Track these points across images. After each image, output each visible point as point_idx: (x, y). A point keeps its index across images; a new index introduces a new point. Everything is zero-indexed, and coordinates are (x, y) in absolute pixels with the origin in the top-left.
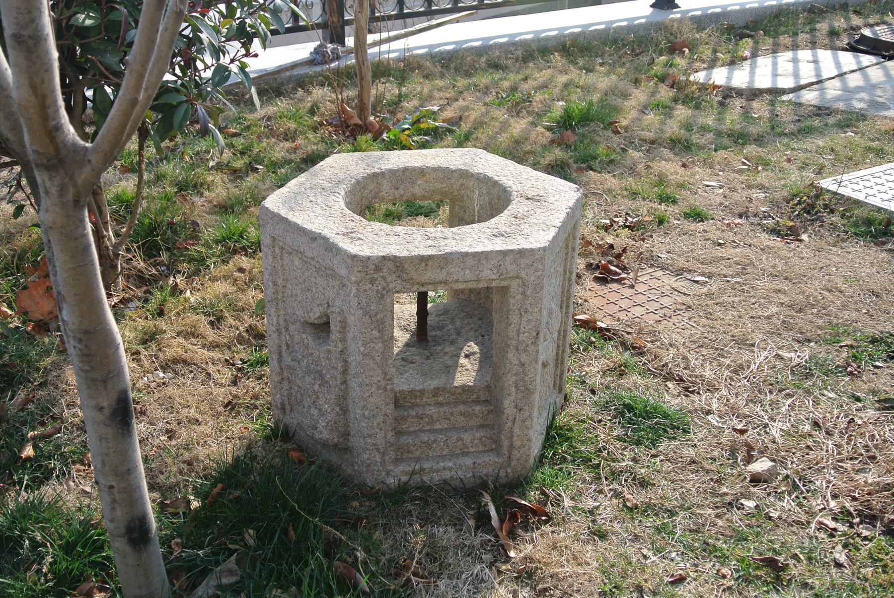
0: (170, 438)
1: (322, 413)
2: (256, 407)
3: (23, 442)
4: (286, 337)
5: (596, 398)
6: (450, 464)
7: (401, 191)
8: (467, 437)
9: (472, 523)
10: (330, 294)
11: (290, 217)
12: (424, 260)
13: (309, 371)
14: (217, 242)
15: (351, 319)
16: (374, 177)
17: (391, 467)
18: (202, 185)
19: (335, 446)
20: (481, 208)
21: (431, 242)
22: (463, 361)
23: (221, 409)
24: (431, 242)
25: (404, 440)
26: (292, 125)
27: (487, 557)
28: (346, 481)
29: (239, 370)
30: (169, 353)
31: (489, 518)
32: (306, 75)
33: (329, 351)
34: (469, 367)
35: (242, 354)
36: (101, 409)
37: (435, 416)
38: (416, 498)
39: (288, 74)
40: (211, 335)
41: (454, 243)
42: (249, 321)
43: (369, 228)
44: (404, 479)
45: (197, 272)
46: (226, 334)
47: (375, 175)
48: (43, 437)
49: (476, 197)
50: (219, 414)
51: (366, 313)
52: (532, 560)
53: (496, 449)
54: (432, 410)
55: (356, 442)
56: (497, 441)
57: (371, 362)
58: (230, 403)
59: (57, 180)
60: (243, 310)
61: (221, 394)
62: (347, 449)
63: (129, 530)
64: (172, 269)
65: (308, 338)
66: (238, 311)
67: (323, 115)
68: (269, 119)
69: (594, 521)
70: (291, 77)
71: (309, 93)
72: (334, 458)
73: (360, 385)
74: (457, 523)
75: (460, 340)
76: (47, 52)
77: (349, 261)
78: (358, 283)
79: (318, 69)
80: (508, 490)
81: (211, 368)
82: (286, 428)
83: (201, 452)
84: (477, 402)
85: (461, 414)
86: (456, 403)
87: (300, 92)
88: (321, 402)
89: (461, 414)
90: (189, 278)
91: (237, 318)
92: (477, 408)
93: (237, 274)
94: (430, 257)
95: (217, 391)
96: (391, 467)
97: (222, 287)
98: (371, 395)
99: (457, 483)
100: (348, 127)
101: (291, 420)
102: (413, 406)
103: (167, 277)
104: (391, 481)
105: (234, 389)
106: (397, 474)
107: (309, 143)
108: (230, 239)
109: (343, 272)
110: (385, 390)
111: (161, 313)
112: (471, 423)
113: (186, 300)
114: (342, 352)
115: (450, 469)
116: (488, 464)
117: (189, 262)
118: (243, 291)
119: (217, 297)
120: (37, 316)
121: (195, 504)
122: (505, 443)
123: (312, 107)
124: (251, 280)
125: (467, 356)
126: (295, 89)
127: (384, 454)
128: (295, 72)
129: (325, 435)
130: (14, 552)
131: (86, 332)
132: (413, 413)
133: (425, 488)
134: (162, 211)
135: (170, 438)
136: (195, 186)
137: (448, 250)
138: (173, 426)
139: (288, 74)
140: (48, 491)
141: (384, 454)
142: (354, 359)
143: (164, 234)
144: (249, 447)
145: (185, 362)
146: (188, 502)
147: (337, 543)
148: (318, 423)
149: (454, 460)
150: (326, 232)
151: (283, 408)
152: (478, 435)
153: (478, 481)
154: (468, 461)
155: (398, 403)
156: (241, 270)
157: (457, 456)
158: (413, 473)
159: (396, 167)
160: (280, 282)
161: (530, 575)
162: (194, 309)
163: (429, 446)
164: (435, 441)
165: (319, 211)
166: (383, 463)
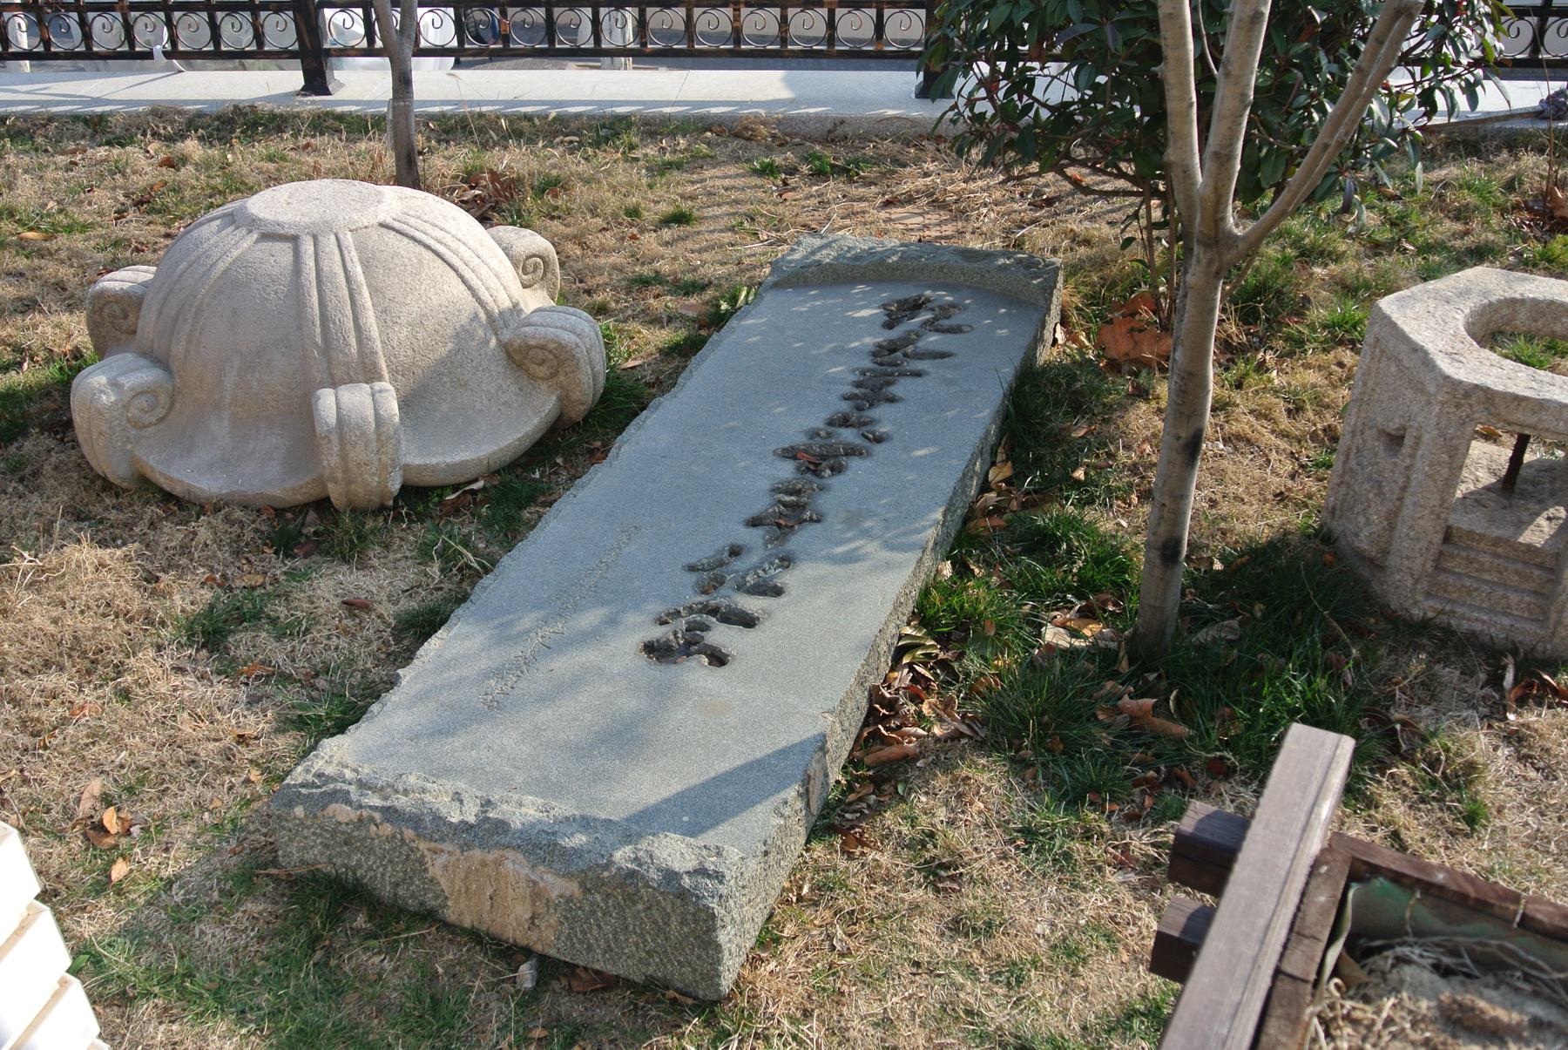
0: (1211, 507)
1: (1368, 523)
2: (1306, 506)
3: (1076, 466)
4: (1358, 441)
6: (1485, 618)
7: (1540, 324)
8: (1514, 598)
9: (1483, 676)
10: (1415, 408)
11: (1399, 323)
12: (1518, 400)
13: (1370, 479)
14: (1325, 327)
15: (1426, 437)
16: (1512, 302)
17: (1420, 598)
18: (1330, 253)
19: (1371, 560)
21: (1534, 384)
23: (1271, 497)
24: (1534, 384)
25: (1442, 577)
26: (1472, 199)
27: (1486, 710)
28: (1368, 597)
29: (1302, 466)
30: (1235, 427)
31: (1503, 678)
32: (1521, 132)
33: (1395, 464)
34: (1546, 529)
35: (1310, 452)
36: (1178, 438)
37: (1487, 565)
38: (1434, 636)
39: (1497, 125)
40: (1285, 423)
41: (1558, 391)
42: (1330, 420)
43: (1475, 354)
44: (1430, 614)
45: (1291, 354)
46: (1300, 426)
47: (1513, 301)
48: (1095, 467)
50: (1266, 501)
51: (1442, 435)
52: (1529, 728)
53: (1542, 622)
55: (1393, 561)
56: (1545, 613)
57: (1431, 484)
58: (1281, 493)
59: (1209, 255)
60: (1328, 407)
61: (1276, 483)
62: (1382, 568)
63: (1165, 546)
64: (1263, 342)
65: (1380, 447)
66: (1321, 405)
67: (1524, 193)
68: (1446, 186)
70: (1500, 130)
71: (1517, 159)
72: (1366, 574)
73: (1414, 504)
74: (1468, 672)
76: (1233, 167)
78: (1443, 404)
79: (1543, 125)
81: (1273, 456)
82: (1330, 531)
83: (1239, 527)
84: (1540, 566)
85: (1516, 572)
86: (1515, 561)
87: (1505, 155)
88: (1371, 511)
89: (1516, 572)
90: (1281, 358)
91: (1316, 413)
92: (1537, 572)
93: (1334, 367)
95: (1271, 478)
96: (1420, 598)
97: (1313, 377)
98: (1422, 518)
99: (1486, 639)
100: (1552, 218)
101: (1337, 526)
102: (1467, 548)
103: (1257, 350)
104: (1415, 611)
105: (1290, 483)
106: (1423, 608)
107: (1490, 229)
108: (1340, 327)
109: (1432, 389)
110: (1438, 516)
111: (1239, 386)
112: (1525, 586)
113: (1270, 380)
114: (1408, 468)
115: (1484, 622)
116: (1528, 632)
117: (1286, 340)
118: (1335, 387)
119: (1304, 386)
120: (1113, 354)
121: (1218, 566)
122: (1553, 616)
123: (1513, 179)
124: (1348, 378)
125: (1549, 519)
126: (1498, 150)
127: (1417, 581)
128: (1508, 125)
129: (1364, 544)
130: (1052, 549)
131: (1190, 374)
132: (1464, 554)
133: (1449, 632)
134: (1276, 274)
135: (1211, 507)
136: (1321, 254)
137: (1548, 396)
138: (1218, 497)
139: (1497, 125)
140: (1090, 514)
141: (1417, 581)
142: (1417, 477)
143: (1268, 302)
144: (1286, 533)
145: (1248, 441)
146: (1212, 563)
147: (1337, 639)
148: (1363, 532)
149: (1487, 613)
150: (1430, 347)
151: (1333, 512)
152: (1527, 599)
153: (1510, 646)
154: (1506, 622)
155: (1448, 537)
156: (1341, 365)
157: (1496, 613)
158: (1442, 612)
159: (1541, 297)
160: (1370, 383)
161: (1520, 740)
162: (1276, 392)
163: (1469, 593)
164: (1476, 590)
165: (1432, 324)
166: (1414, 590)
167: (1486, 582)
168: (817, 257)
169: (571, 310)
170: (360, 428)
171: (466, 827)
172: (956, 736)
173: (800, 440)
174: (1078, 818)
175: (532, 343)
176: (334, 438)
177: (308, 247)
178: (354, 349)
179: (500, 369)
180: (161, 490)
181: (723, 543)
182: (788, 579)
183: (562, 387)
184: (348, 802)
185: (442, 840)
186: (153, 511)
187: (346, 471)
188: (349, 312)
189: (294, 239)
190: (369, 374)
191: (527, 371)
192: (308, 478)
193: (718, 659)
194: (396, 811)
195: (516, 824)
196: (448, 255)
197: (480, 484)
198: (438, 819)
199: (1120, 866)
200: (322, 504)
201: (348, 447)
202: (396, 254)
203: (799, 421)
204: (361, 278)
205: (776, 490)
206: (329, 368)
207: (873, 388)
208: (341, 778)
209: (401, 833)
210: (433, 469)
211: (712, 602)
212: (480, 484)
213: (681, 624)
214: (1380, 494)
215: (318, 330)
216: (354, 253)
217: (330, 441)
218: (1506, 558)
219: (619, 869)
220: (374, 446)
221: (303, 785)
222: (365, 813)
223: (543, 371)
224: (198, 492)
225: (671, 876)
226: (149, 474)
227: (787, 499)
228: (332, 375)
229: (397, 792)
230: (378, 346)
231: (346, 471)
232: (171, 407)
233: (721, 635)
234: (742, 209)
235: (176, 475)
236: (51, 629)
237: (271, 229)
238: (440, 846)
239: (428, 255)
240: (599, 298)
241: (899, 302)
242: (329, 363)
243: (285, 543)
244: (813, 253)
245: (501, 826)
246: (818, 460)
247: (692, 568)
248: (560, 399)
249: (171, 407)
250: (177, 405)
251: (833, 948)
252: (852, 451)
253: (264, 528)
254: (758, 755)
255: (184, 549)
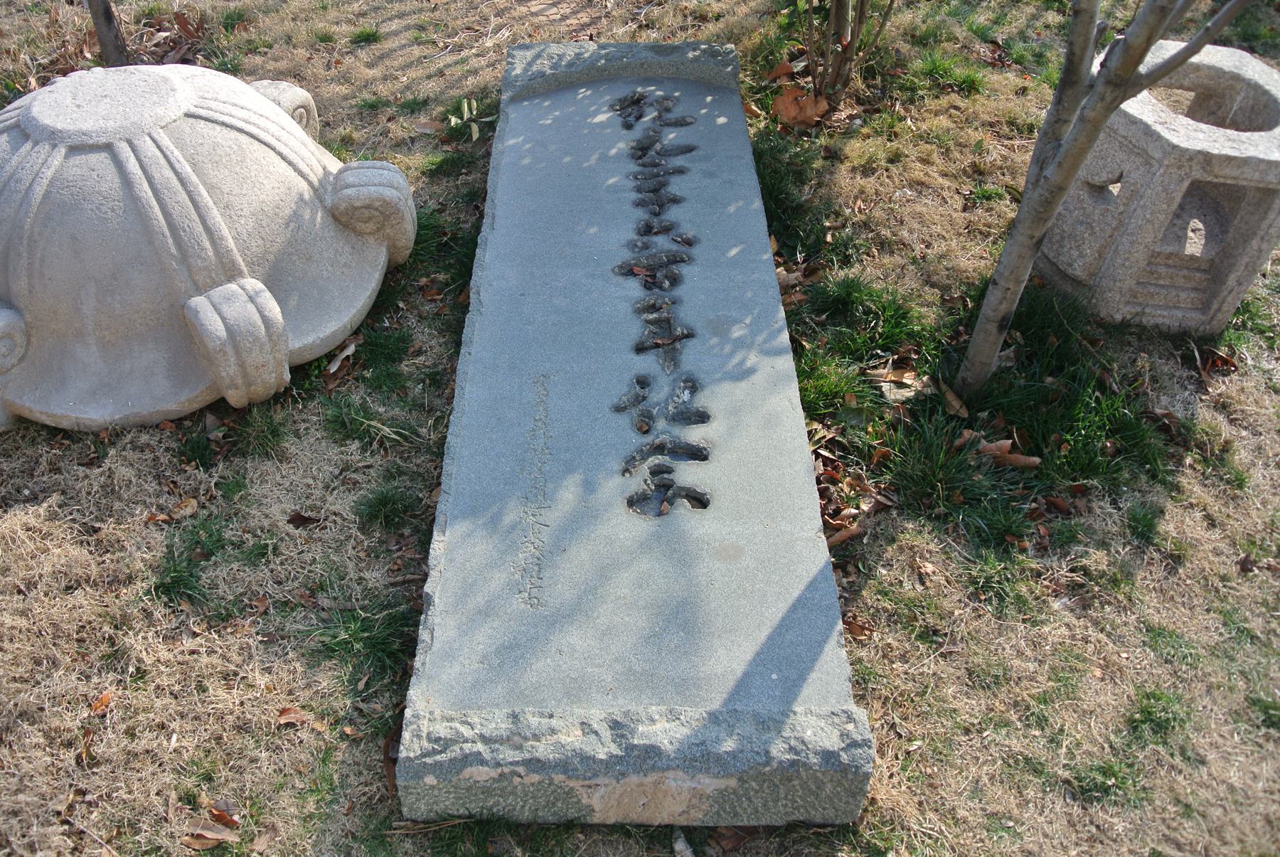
1: (1081, 256)
5: (1267, 282)
8: (1183, 295)
12: (1229, 159)
17: (1121, 306)
20: (1240, 108)
22: (1191, 234)
44: (1129, 317)
49: (1239, 98)
54: (1162, 270)
69: (1270, 379)
75: (1185, 216)
77: (1170, 149)
78: (1168, 166)
80: (1210, 340)
84: (1198, 270)
85: (1184, 277)
86: (1181, 268)
89: (1184, 277)
92: (1198, 275)
94: (1235, 158)
96: (1121, 306)
99: (1165, 329)
115: (1164, 317)
122: (1215, 306)
125: (1193, 231)
129: (1078, 271)
154: (1179, 314)
158: (1137, 314)
167: (1163, 286)
168: (534, 68)
169: (378, 163)
170: (252, 334)
171: (613, 760)
172: (879, 508)
173: (626, 255)
174: (1013, 562)
175: (358, 204)
176: (229, 350)
177: (124, 150)
178: (211, 253)
179: (332, 234)
180: (45, 427)
181: (628, 377)
182: (703, 401)
183: (389, 238)
184: (483, 762)
185: (595, 775)
186: (46, 453)
187: (245, 375)
188: (195, 216)
189: (108, 147)
190: (232, 273)
191: (354, 230)
192: (202, 387)
193: (700, 501)
194: (539, 761)
195: (665, 745)
196: (262, 135)
197: (351, 350)
198: (586, 759)
199: (1057, 595)
200: (219, 406)
201: (244, 355)
202: (215, 146)
203: (616, 233)
204: (194, 178)
205: (639, 311)
206: (190, 276)
207: (655, 195)
208: (458, 739)
209: (551, 780)
210: (311, 347)
211: (657, 441)
212: (351, 350)
213: (644, 469)
214: (1093, 233)
215: (170, 241)
216: (176, 152)
217: (225, 353)
218: (1175, 266)
219: (781, 762)
220: (268, 347)
221: (424, 755)
222: (506, 770)
223: (370, 227)
224: (88, 423)
225: (828, 756)
226: (26, 414)
227: (651, 317)
228: (195, 283)
229: (526, 739)
230: (231, 243)
231: (245, 375)
232: (29, 342)
233: (688, 474)
234: (412, 20)
235: (59, 412)
236: (22, 622)
237: (77, 141)
238: (594, 782)
239: (244, 139)
240: (342, 131)
241: (620, 100)
242: (189, 270)
243: (201, 454)
244: (530, 64)
245: (652, 751)
246: (657, 273)
247: (619, 409)
248: (388, 249)
249: (29, 342)
250: (34, 340)
251: (900, 736)
252: (676, 260)
253: (174, 445)
254: (796, 594)
255: (109, 490)
